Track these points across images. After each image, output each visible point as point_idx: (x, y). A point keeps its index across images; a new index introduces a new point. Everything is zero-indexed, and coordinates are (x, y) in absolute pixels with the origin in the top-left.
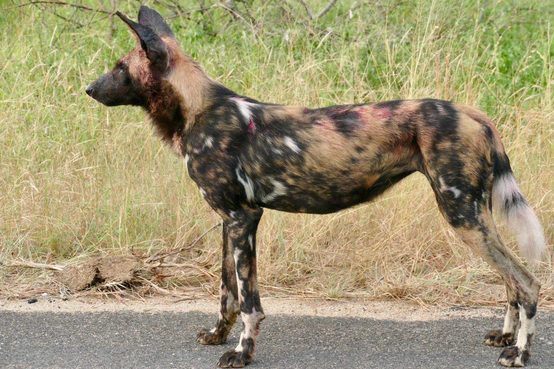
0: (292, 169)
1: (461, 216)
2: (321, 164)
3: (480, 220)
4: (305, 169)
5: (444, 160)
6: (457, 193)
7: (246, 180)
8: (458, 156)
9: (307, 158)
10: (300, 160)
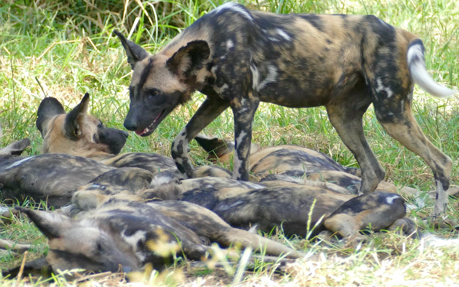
0: (285, 55)
1: (391, 114)
2: (307, 51)
3: (404, 115)
4: (295, 54)
5: (383, 64)
6: (390, 93)
7: (254, 69)
8: (394, 61)
9: (296, 44)
10: (291, 48)
